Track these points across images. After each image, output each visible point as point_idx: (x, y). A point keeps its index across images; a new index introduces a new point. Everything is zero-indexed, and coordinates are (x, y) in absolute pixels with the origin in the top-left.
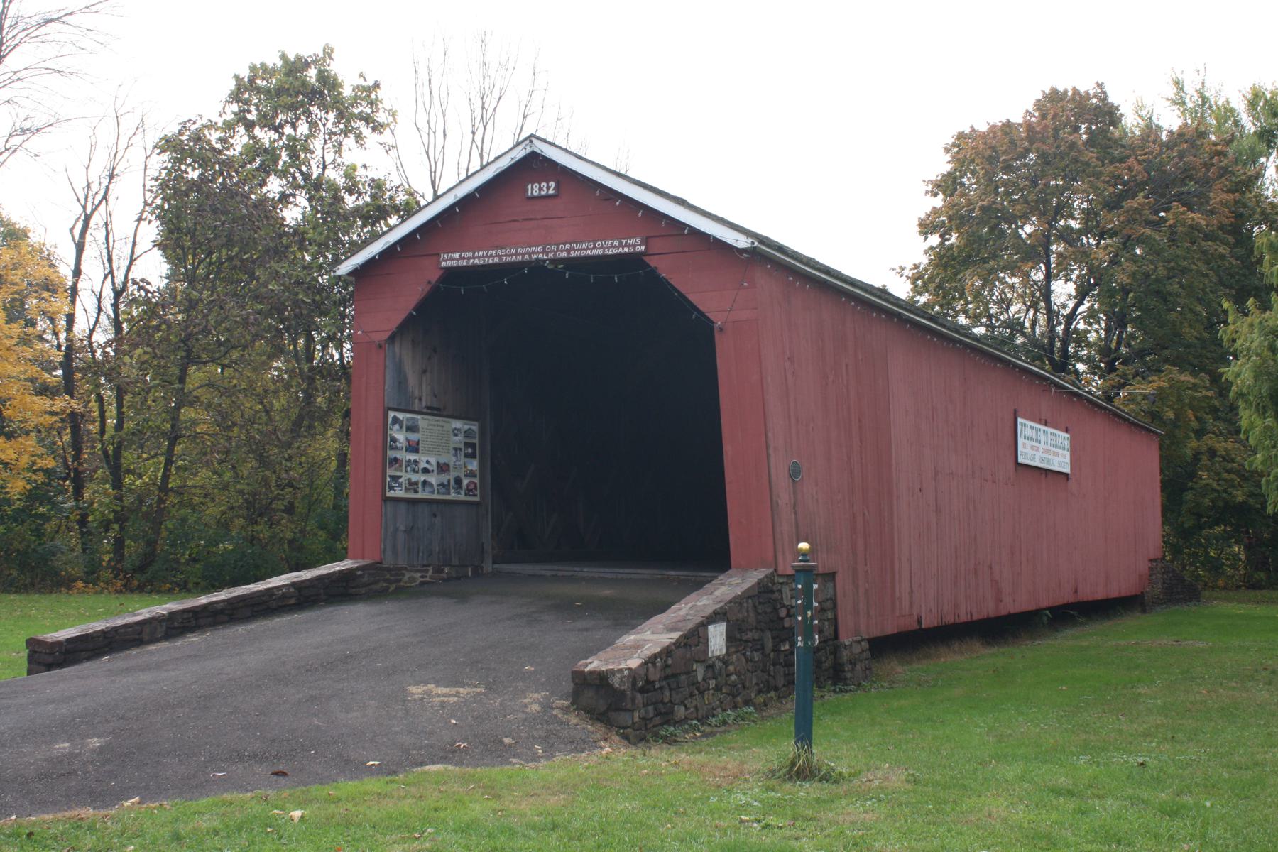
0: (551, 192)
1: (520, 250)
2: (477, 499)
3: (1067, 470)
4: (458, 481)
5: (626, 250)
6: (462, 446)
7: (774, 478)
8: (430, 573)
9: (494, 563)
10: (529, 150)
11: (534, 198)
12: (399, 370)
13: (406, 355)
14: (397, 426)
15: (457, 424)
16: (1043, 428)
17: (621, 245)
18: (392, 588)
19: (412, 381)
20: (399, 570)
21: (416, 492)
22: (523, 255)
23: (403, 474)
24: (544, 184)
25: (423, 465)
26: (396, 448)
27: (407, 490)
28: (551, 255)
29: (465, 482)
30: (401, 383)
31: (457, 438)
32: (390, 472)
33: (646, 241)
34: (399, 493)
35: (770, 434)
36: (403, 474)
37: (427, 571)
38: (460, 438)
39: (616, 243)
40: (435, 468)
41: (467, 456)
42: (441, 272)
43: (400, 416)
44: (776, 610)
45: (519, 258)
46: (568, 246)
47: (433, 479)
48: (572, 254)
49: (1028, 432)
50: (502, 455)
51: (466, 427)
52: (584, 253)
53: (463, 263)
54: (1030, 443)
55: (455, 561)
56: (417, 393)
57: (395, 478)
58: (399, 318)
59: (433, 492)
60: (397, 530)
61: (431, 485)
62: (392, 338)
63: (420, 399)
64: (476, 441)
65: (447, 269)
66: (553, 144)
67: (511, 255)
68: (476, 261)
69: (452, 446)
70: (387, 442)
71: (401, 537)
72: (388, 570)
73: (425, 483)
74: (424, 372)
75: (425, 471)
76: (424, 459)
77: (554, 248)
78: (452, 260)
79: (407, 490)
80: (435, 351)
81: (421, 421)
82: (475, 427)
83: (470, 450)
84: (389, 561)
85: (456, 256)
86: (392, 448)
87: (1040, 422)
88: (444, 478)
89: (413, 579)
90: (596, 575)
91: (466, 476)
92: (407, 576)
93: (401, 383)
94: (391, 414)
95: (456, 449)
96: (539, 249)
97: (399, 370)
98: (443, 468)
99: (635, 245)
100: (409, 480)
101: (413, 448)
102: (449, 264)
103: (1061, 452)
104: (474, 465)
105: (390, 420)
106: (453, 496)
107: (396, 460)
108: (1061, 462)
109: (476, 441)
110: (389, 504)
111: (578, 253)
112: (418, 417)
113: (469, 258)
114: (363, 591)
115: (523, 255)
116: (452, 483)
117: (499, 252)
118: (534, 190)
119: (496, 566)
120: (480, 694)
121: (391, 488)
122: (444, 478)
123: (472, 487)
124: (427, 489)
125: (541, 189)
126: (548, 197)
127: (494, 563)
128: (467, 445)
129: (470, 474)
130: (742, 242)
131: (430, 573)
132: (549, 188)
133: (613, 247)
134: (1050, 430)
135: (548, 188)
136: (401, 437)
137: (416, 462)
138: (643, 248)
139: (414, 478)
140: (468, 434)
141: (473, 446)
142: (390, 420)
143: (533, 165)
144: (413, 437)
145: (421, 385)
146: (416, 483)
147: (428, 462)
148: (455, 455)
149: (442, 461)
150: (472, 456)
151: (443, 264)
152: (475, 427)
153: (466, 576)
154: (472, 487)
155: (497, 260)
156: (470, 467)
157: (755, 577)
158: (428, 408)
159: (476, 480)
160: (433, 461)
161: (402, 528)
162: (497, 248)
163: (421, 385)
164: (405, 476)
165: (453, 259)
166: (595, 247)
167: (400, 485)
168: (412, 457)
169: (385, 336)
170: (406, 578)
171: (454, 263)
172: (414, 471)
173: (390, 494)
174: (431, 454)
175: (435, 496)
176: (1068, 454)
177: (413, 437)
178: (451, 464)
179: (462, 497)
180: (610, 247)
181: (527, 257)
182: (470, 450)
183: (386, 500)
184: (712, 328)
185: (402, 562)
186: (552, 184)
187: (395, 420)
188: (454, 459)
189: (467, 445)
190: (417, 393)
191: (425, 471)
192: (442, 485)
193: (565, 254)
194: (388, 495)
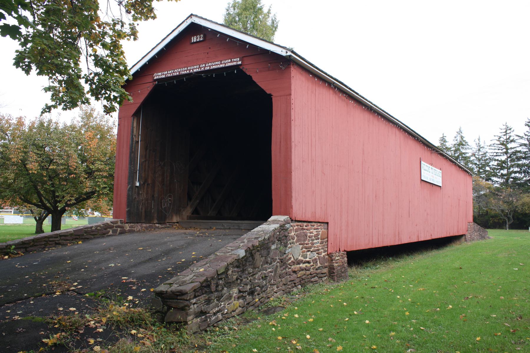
0: (201, 39)
3: (441, 185)
11: (194, 43)
16: (431, 167)
17: (231, 62)
24: (198, 36)
39: (230, 60)
48: (212, 68)
49: (427, 168)
53: (164, 76)
54: (426, 172)
66: (206, 19)
67: (184, 71)
68: (169, 75)
85: (160, 74)
87: (430, 164)
99: (237, 61)
103: (438, 177)
108: (438, 181)
118: (194, 39)
120: (153, 287)
125: (197, 38)
126: (200, 41)
130: (283, 53)
134: (434, 168)
135: (200, 38)
138: (240, 63)
143: (193, 29)
151: (155, 78)
155: (178, 73)
165: (159, 75)
171: (160, 77)
176: (441, 178)
180: (228, 63)
186: (202, 36)
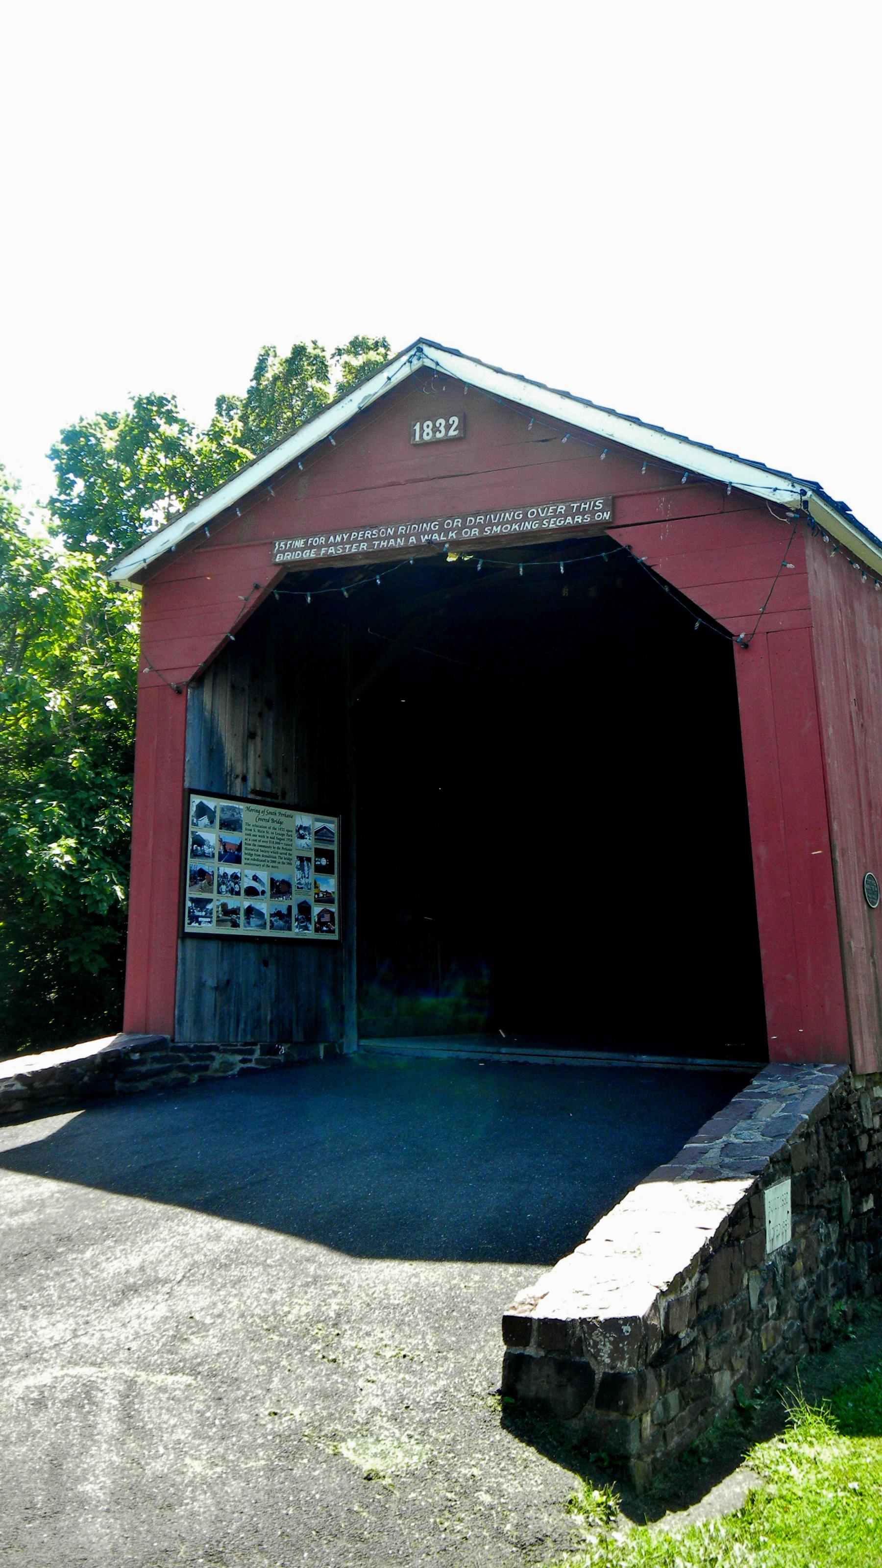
0: (452, 433)
1: (401, 529)
2: (335, 937)
4: (305, 909)
5: (579, 519)
6: (312, 855)
7: (843, 904)
8: (257, 1055)
9: (361, 1036)
10: (416, 364)
12: (211, 734)
13: (219, 706)
14: (205, 820)
15: (304, 819)
17: (569, 512)
18: (195, 1078)
19: (230, 750)
20: (204, 1052)
21: (235, 925)
22: (407, 537)
23: (213, 895)
25: (247, 882)
26: (203, 855)
27: (220, 922)
28: (452, 535)
29: (316, 910)
30: (213, 752)
31: (303, 842)
32: (192, 893)
33: (613, 504)
34: (207, 927)
35: (835, 826)
36: (213, 895)
37: (252, 1052)
38: (309, 841)
39: (562, 508)
40: (267, 888)
41: (319, 869)
42: (275, 571)
43: (211, 803)
44: (854, 1141)
45: (401, 542)
46: (480, 519)
47: (264, 906)
48: (488, 531)
50: (360, 862)
51: (319, 825)
52: (507, 529)
53: (310, 554)
55: (298, 1037)
56: (239, 769)
57: (200, 903)
58: (209, 646)
59: (263, 926)
60: (201, 985)
61: (261, 915)
62: (198, 680)
63: (244, 779)
64: (334, 847)
65: (284, 565)
68: (332, 550)
69: (296, 853)
70: (187, 846)
71: (209, 997)
72: (185, 1049)
73: (250, 911)
74: (252, 736)
75: (251, 892)
76: (250, 873)
77: (458, 522)
78: (292, 550)
79: (220, 922)
80: (269, 704)
81: (247, 813)
82: (333, 825)
83: (324, 861)
84: (187, 1035)
85: (300, 543)
86: (195, 854)
88: (282, 904)
89: (230, 1065)
90: (522, 1059)
91: (317, 901)
92: (219, 1057)
93: (213, 752)
94: (196, 800)
95: (301, 859)
96: (434, 526)
97: (211, 734)
98: (280, 888)
100: (224, 905)
101: (232, 855)
102: (289, 557)
104: (330, 885)
105: (193, 809)
106: (296, 932)
107: (202, 874)
109: (334, 847)
110: (189, 943)
111: (497, 530)
112: (241, 806)
113: (319, 547)
114: (142, 1086)
115: (407, 537)
116: (295, 911)
117: (368, 534)
118: (424, 431)
119: (364, 1042)
121: (194, 919)
122: (282, 904)
123: (327, 918)
124: (254, 921)
125: (436, 430)
126: (448, 441)
127: (361, 1036)
128: (319, 853)
129: (327, 899)
130: (785, 495)
131: (257, 1055)
132: (446, 427)
133: (556, 516)
135: (448, 427)
136: (211, 837)
137: (235, 877)
138: (607, 516)
139: (233, 903)
140: (321, 835)
141: (328, 854)
142: (193, 809)
144: (233, 838)
145: (245, 756)
146: (235, 911)
147: (255, 878)
148: (301, 868)
149: (279, 877)
150: (327, 870)
151: (279, 558)
152: (333, 825)
153: (316, 1060)
154: (327, 918)
155: (364, 546)
156: (323, 888)
157: (815, 1088)
158: (254, 792)
159: (334, 908)
160: (264, 876)
161: (211, 982)
162: (364, 528)
163: (245, 756)
164: (217, 900)
165: (295, 551)
166: (525, 518)
167: (209, 914)
168: (230, 869)
169: (186, 676)
170: (216, 1065)
171: (296, 556)
172: (232, 891)
173: (192, 928)
174: (262, 861)
175: (267, 933)
177: (233, 838)
178: (294, 883)
179: (310, 934)
180: (551, 518)
181: (413, 540)
182: (324, 861)
183: (185, 936)
184: (730, 644)
185: (209, 1039)
187: (202, 810)
188: (298, 874)
189: (319, 853)
190: (239, 769)
191: (251, 892)
192: (278, 914)
193: (475, 532)
194: (188, 929)
